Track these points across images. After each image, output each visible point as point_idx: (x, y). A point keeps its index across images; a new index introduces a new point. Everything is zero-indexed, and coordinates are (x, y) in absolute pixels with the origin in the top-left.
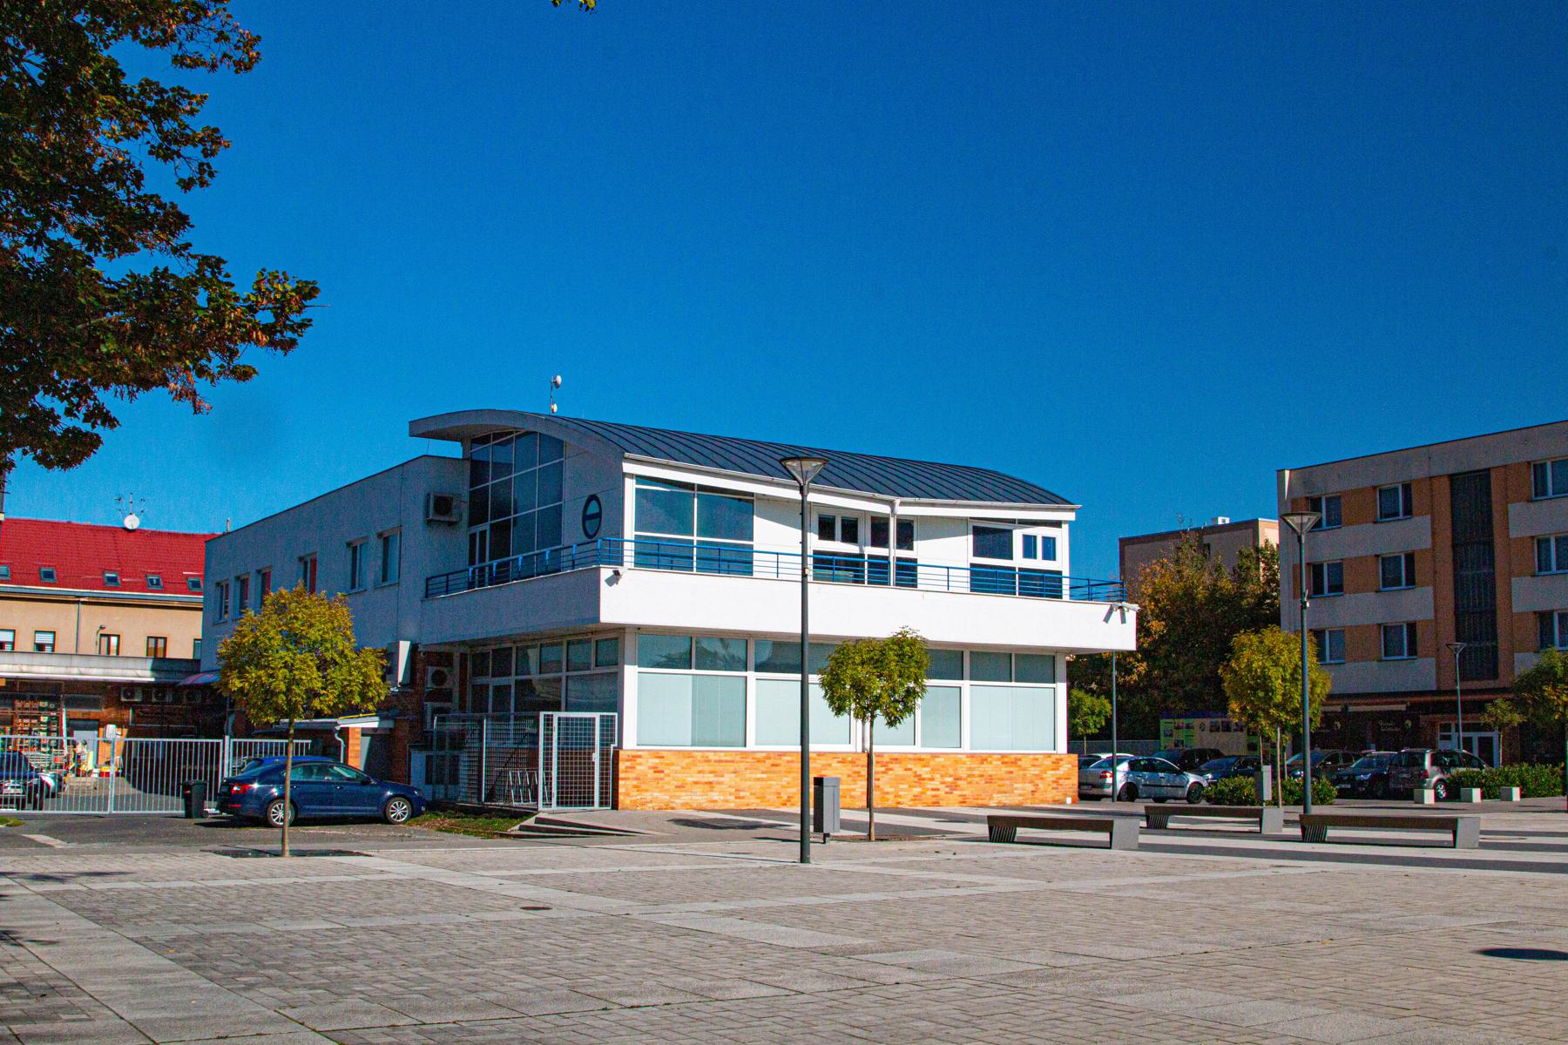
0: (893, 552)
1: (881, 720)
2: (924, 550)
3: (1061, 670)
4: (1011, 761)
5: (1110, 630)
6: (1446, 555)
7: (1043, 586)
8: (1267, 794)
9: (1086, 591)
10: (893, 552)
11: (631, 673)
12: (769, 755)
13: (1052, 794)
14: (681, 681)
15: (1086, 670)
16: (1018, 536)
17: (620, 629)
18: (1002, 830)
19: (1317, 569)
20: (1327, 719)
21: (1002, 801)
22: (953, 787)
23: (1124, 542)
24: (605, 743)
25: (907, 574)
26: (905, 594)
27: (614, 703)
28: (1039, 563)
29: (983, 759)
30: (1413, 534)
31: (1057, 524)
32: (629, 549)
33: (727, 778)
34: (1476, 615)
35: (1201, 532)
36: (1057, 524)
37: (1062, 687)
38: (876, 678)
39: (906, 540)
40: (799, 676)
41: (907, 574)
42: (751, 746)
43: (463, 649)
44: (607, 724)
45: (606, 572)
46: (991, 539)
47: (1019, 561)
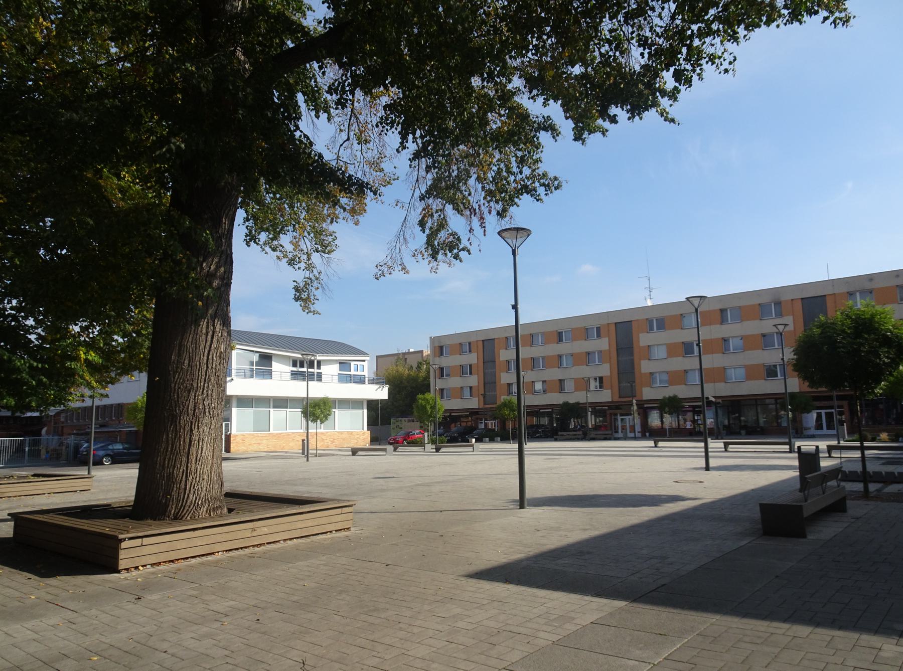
0: (315, 370)
1: (319, 422)
2: (324, 369)
3: (365, 406)
4: (351, 434)
5: (381, 393)
6: (481, 364)
7: (360, 380)
8: (426, 441)
9: (372, 382)
10: (315, 370)
11: (235, 411)
12: (277, 434)
13: (363, 443)
14: (249, 412)
15: (372, 405)
16: (352, 364)
17: (231, 396)
18: (354, 452)
19: (442, 369)
20: (445, 418)
21: (354, 444)
22: (333, 442)
23: (378, 357)
24: (226, 432)
25: (319, 377)
26: (319, 383)
27: (228, 419)
28: (359, 373)
29: (342, 433)
30: (472, 358)
31: (364, 361)
32: (234, 372)
33: (264, 442)
34: (489, 383)
35: (404, 354)
36: (364, 361)
37: (365, 411)
38: (316, 410)
39: (319, 367)
40: (702, 444)
41: (319, 377)
42: (271, 431)
43: (616, 435)
44: (227, 426)
45: (228, 379)
46: (344, 365)
47: (353, 372)
